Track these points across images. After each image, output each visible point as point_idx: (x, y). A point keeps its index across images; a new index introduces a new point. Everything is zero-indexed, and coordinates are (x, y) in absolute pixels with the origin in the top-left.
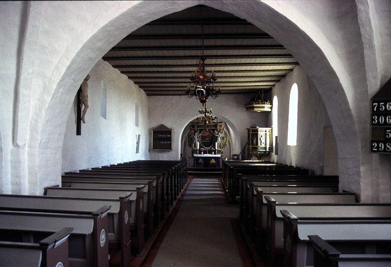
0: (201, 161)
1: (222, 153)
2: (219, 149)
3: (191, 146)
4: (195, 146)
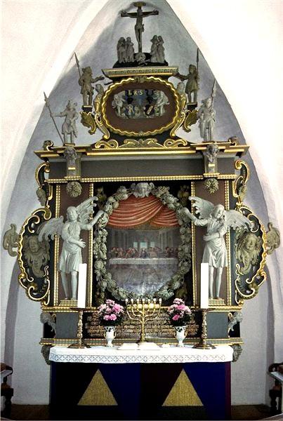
0: (98, 393)
1: (236, 333)
2: (222, 307)
3: (39, 289)
4: (68, 292)
